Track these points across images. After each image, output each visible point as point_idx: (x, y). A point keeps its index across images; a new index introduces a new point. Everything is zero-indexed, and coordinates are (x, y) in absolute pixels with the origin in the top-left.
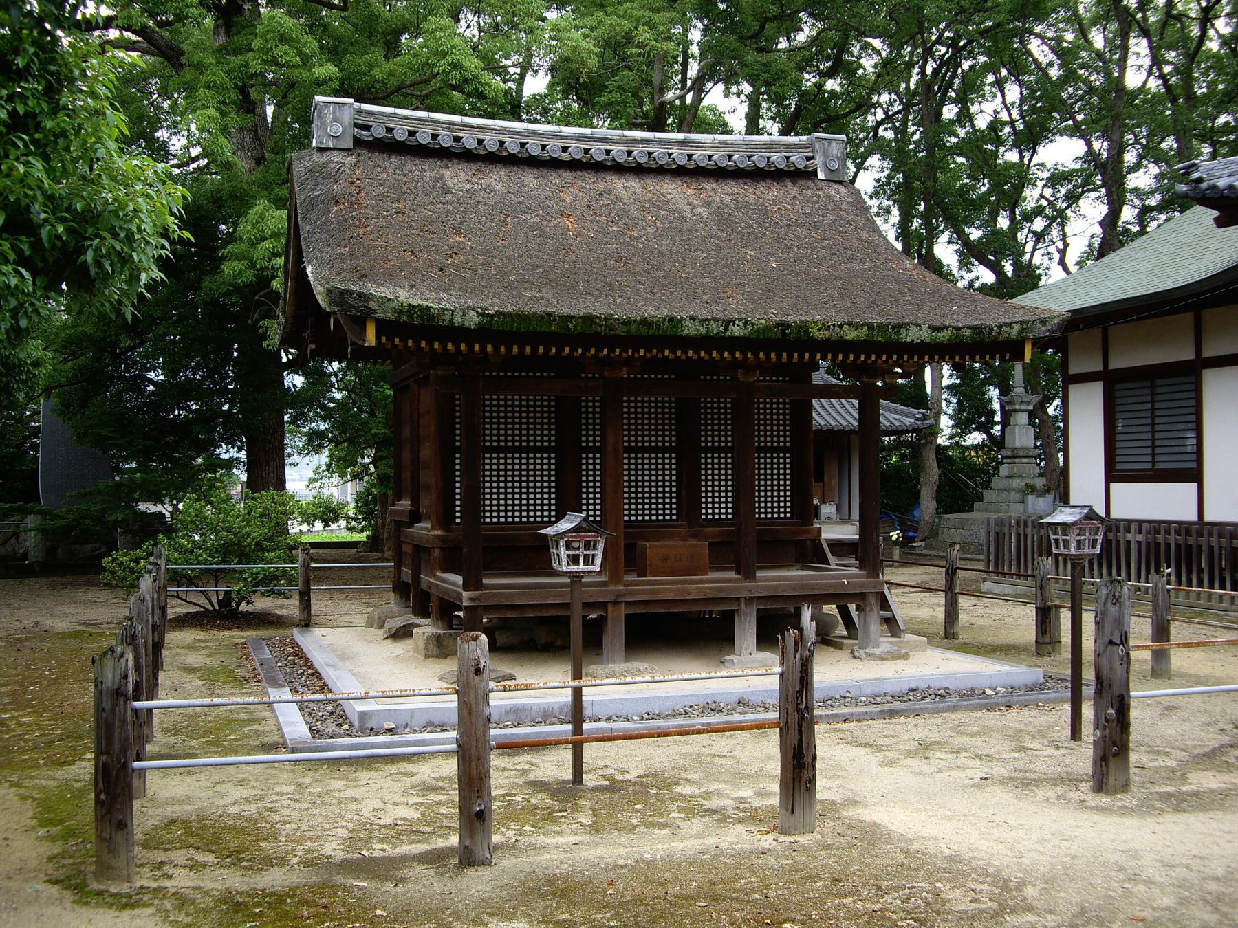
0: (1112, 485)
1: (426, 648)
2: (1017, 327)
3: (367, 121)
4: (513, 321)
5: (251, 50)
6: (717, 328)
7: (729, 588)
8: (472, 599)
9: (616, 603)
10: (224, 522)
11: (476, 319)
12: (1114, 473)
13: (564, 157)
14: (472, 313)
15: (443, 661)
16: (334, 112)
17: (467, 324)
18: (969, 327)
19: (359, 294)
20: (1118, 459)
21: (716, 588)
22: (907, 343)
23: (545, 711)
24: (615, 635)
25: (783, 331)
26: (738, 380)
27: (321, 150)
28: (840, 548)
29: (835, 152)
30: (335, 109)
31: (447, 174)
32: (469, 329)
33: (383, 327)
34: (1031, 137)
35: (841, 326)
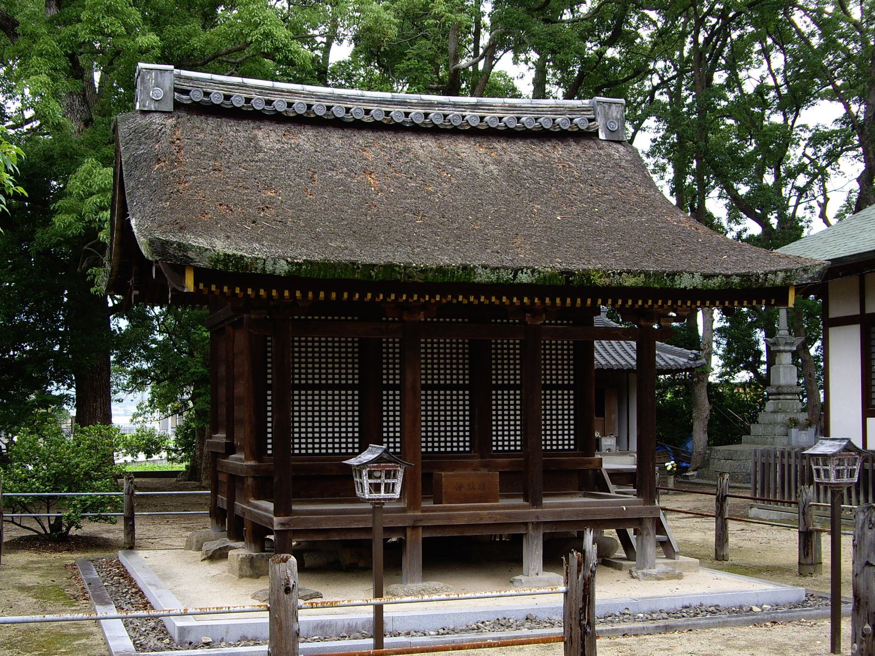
1: (241, 569)
2: (781, 275)
3: (186, 86)
4: (320, 269)
5: (80, 21)
6: (506, 276)
7: (518, 514)
8: (282, 524)
9: (414, 527)
10: (55, 453)
11: (286, 268)
13: (366, 119)
15: (256, 581)
16: (156, 78)
17: (277, 272)
18: (737, 275)
19: (179, 244)
21: (507, 514)
23: (349, 626)
24: (413, 556)
25: (567, 278)
26: (526, 323)
27: (144, 113)
28: (619, 477)
31: (260, 134)
32: (279, 276)
33: (201, 274)
34: (795, 101)
35: (620, 274)
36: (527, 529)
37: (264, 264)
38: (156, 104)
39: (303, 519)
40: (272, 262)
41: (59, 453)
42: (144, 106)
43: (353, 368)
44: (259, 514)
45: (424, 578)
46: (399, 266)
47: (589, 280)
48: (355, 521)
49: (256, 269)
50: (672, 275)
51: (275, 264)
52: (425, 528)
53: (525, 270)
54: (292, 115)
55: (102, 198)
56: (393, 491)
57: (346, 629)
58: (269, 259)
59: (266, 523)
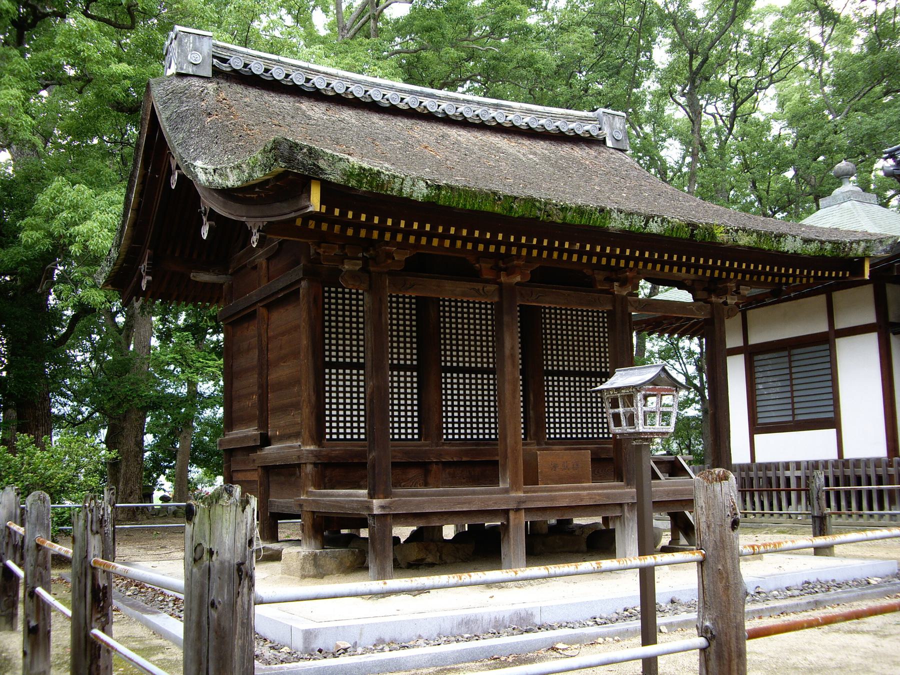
0: (755, 436)
1: (303, 568)
2: (863, 244)
3: (224, 54)
4: (460, 195)
5: (54, 45)
6: (638, 223)
7: (614, 494)
8: (382, 507)
9: (517, 510)
10: (29, 464)
11: (425, 191)
12: (756, 427)
13: (401, 106)
14: (422, 184)
15: (322, 581)
16: (194, 43)
17: (415, 195)
18: (830, 242)
19: (310, 149)
20: (759, 415)
21: (605, 494)
22: (783, 252)
23: (496, 621)
24: (515, 544)
25: (692, 230)
27: (180, 75)
29: (618, 125)
30: (194, 39)
31: (303, 107)
32: (416, 201)
33: (330, 192)
35: (737, 231)
36: (623, 511)
37: (402, 184)
38: (195, 68)
39: (405, 501)
40: (411, 183)
41: (34, 464)
42: (182, 69)
43: (411, 348)
44: (337, 502)
45: (527, 566)
46: (540, 202)
47: (713, 236)
48: (459, 503)
49: (393, 189)
50: (779, 236)
51: (413, 185)
52: (528, 510)
53: (656, 218)
54: (330, 94)
55: (73, 214)
56: (668, 425)
57: (492, 624)
58: (408, 179)
59: (358, 509)
